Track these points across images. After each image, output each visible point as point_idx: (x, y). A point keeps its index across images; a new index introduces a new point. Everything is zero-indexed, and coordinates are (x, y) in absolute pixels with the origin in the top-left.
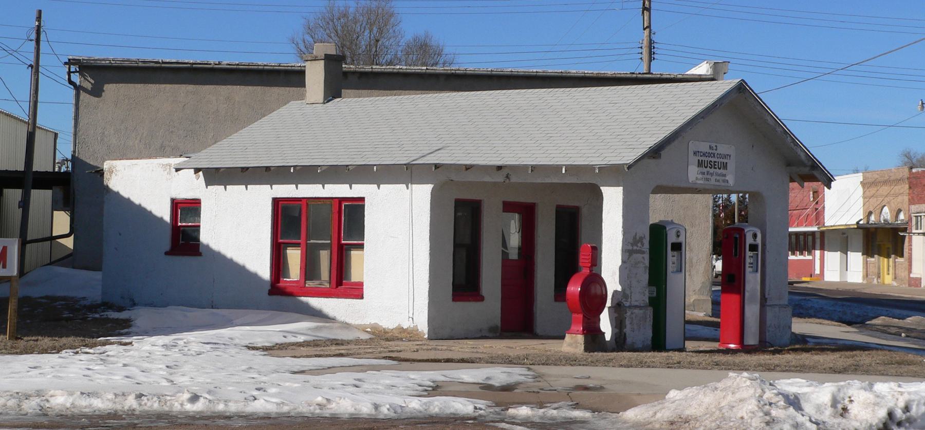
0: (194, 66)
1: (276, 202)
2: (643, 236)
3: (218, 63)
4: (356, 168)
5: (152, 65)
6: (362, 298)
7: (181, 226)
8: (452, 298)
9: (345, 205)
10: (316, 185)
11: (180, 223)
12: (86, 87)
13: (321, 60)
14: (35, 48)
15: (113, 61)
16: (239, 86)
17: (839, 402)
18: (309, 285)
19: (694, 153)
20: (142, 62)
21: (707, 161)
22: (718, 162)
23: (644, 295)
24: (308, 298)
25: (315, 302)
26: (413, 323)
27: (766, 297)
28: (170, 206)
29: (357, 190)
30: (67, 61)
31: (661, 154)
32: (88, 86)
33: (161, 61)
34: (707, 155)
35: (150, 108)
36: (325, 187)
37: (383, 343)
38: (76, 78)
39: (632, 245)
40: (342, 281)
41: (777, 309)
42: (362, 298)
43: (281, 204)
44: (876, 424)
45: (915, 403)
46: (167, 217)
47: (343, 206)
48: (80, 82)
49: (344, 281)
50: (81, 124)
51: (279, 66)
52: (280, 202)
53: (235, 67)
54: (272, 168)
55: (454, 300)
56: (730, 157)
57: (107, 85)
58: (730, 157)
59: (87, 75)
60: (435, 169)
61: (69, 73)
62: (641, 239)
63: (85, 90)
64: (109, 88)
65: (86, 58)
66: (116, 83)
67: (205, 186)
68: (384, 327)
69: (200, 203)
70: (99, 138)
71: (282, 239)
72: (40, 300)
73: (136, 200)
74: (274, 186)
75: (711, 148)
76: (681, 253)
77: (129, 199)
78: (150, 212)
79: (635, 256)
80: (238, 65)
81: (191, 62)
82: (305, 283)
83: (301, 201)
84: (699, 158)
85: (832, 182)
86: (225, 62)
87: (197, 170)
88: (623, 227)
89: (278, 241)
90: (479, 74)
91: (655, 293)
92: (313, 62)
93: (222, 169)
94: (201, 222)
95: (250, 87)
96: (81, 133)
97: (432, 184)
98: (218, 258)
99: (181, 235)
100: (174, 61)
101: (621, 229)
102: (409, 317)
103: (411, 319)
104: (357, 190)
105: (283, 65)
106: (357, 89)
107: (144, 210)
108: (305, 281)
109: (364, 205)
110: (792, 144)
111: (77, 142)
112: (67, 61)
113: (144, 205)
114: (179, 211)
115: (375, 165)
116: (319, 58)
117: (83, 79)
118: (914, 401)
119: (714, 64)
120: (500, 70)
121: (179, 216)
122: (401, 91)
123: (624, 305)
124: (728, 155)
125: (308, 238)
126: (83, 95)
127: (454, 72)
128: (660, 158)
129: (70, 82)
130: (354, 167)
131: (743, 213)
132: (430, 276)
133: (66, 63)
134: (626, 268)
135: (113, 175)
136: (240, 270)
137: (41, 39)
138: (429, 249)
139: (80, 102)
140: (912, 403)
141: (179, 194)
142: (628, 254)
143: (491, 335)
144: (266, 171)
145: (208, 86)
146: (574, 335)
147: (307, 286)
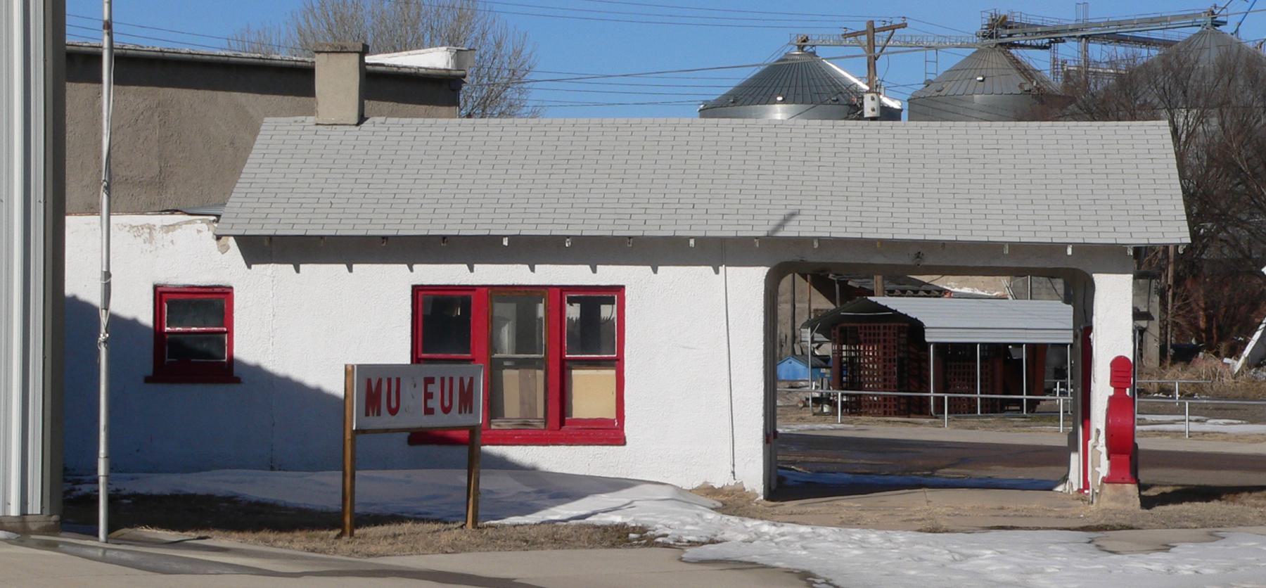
1: (417, 290)
6: (624, 443)
7: (169, 333)
9: (568, 298)
10: (515, 266)
13: (355, 52)
24: (501, 447)
26: (735, 479)
29: (607, 275)
40: (564, 418)
46: (147, 318)
47: (566, 299)
49: (567, 418)
71: (423, 353)
74: (415, 267)
82: (490, 423)
83: (475, 290)
90: (245, 62)
92: (330, 55)
97: (767, 266)
104: (607, 275)
114: (166, 306)
116: (349, 50)
119: (456, 53)
120: (172, 51)
121: (166, 315)
137: (67, 12)
146: (1120, 485)
147: (493, 427)
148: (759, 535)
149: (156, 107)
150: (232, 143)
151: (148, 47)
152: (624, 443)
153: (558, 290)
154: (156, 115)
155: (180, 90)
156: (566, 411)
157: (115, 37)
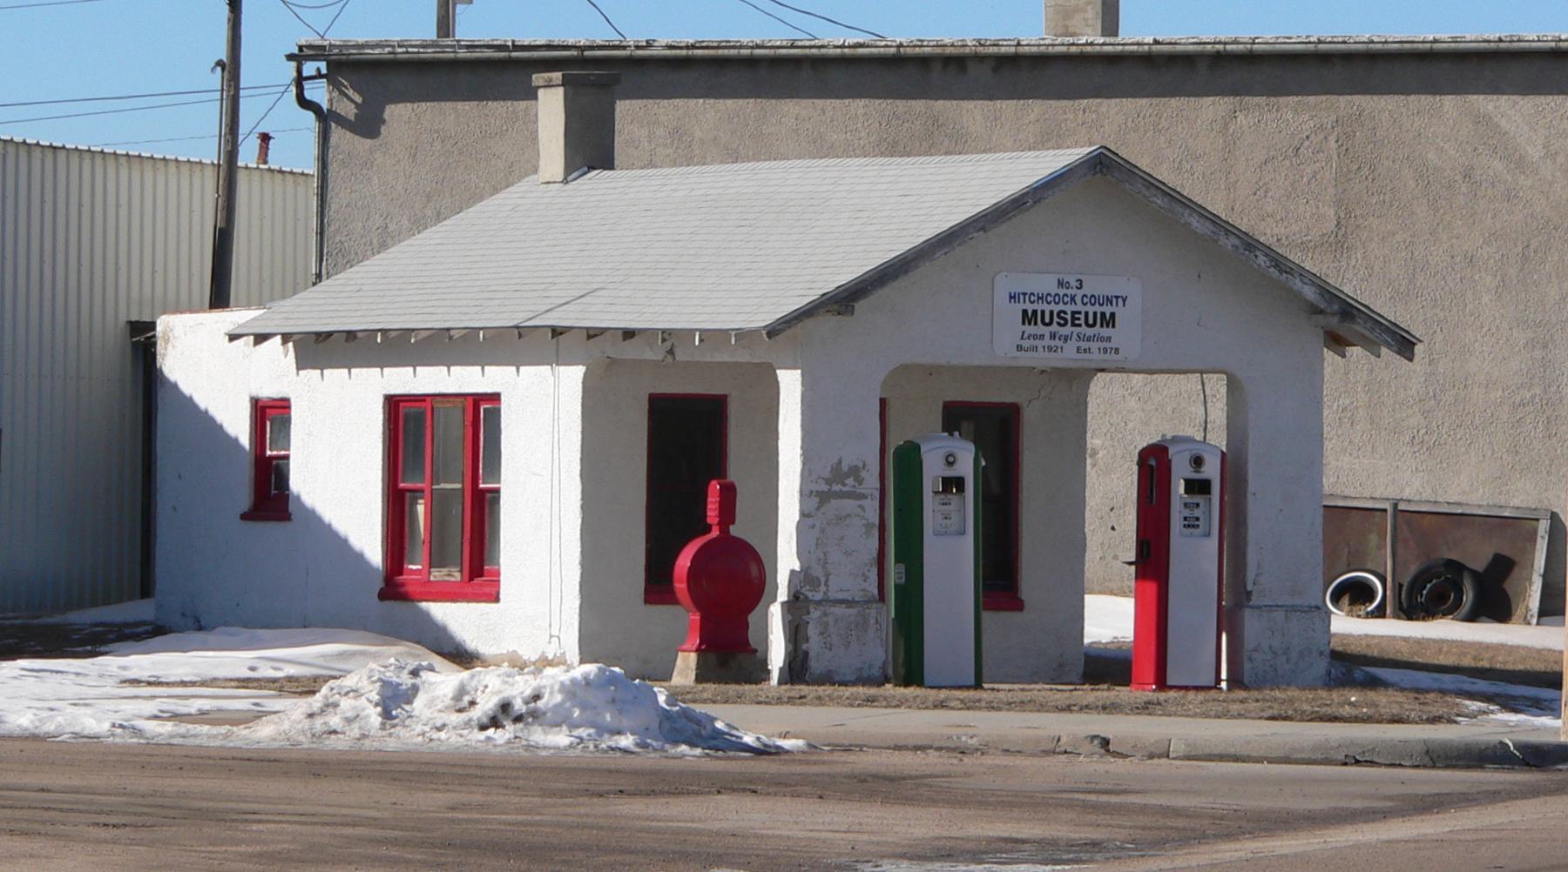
0: (587, 53)
1: (394, 405)
2: (861, 465)
3: (644, 44)
4: (300, 339)
5: (489, 54)
6: (496, 599)
8: (643, 597)
9: (485, 410)
11: (271, 450)
12: (343, 114)
14: (229, 20)
15: (400, 46)
16: (701, 101)
17: (468, 693)
18: (435, 577)
19: (1011, 297)
20: (468, 47)
21: (1095, 314)
22: (1087, 313)
23: (865, 581)
25: (440, 611)
27: (1249, 589)
28: (248, 414)
30: (296, 51)
31: (853, 306)
32: (348, 110)
33: (510, 44)
34: (1049, 299)
35: (493, 162)
36: (385, 374)
38: (318, 92)
39: (828, 481)
40: (483, 567)
41: (1279, 615)
42: (496, 599)
43: (404, 407)
44: (479, 719)
45: (548, 690)
46: (245, 440)
48: (331, 101)
49: (486, 567)
50: (332, 206)
51: (792, 47)
52: (401, 404)
53: (684, 52)
54: (360, 335)
55: (646, 601)
56: (1124, 301)
57: (393, 106)
58: (1124, 301)
59: (346, 83)
60: (553, 337)
61: (300, 80)
62: (855, 472)
63: (342, 121)
64: (396, 113)
65: (338, 43)
66: (412, 101)
67: (295, 370)
68: (525, 658)
69: (289, 407)
70: (375, 241)
73: (202, 402)
74: (522, 369)
75: (1060, 284)
76: (1210, 499)
77: (190, 399)
78: (221, 427)
79: (834, 503)
80: (693, 47)
81: (582, 44)
82: (430, 573)
83: (424, 400)
85: (1416, 347)
86: (663, 41)
87: (286, 338)
88: (802, 448)
89: (478, 485)
91: (903, 580)
93: (393, 334)
94: (292, 448)
95: (729, 102)
96: (332, 228)
98: (312, 518)
99: (273, 477)
100: (543, 43)
101: (799, 451)
102: (551, 636)
103: (555, 640)
105: (800, 44)
106: (990, 99)
107: (212, 420)
108: (430, 567)
109: (499, 411)
110: (1272, 269)
111: (325, 251)
112: (296, 51)
113: (213, 412)
114: (268, 424)
115: (481, 329)
117: (335, 94)
118: (545, 687)
122: (1099, 100)
123: (806, 597)
124: (1117, 297)
125: (434, 479)
126: (338, 134)
127: (1220, 47)
128: (853, 314)
129: (304, 103)
130: (464, 332)
132: (582, 552)
133: (290, 57)
134: (813, 527)
135: (170, 347)
136: (341, 544)
138: (579, 497)
139: (331, 150)
140: (543, 691)
141: (261, 388)
142: (817, 499)
144: (346, 341)
145: (627, 102)
148: (767, 737)
149: (1333, 128)
150: (1467, 176)
151: (1299, 37)
152: (646, 601)
153: (470, 399)
154: (1332, 139)
155: (1375, 98)
156: (486, 556)
157: (541, 84)
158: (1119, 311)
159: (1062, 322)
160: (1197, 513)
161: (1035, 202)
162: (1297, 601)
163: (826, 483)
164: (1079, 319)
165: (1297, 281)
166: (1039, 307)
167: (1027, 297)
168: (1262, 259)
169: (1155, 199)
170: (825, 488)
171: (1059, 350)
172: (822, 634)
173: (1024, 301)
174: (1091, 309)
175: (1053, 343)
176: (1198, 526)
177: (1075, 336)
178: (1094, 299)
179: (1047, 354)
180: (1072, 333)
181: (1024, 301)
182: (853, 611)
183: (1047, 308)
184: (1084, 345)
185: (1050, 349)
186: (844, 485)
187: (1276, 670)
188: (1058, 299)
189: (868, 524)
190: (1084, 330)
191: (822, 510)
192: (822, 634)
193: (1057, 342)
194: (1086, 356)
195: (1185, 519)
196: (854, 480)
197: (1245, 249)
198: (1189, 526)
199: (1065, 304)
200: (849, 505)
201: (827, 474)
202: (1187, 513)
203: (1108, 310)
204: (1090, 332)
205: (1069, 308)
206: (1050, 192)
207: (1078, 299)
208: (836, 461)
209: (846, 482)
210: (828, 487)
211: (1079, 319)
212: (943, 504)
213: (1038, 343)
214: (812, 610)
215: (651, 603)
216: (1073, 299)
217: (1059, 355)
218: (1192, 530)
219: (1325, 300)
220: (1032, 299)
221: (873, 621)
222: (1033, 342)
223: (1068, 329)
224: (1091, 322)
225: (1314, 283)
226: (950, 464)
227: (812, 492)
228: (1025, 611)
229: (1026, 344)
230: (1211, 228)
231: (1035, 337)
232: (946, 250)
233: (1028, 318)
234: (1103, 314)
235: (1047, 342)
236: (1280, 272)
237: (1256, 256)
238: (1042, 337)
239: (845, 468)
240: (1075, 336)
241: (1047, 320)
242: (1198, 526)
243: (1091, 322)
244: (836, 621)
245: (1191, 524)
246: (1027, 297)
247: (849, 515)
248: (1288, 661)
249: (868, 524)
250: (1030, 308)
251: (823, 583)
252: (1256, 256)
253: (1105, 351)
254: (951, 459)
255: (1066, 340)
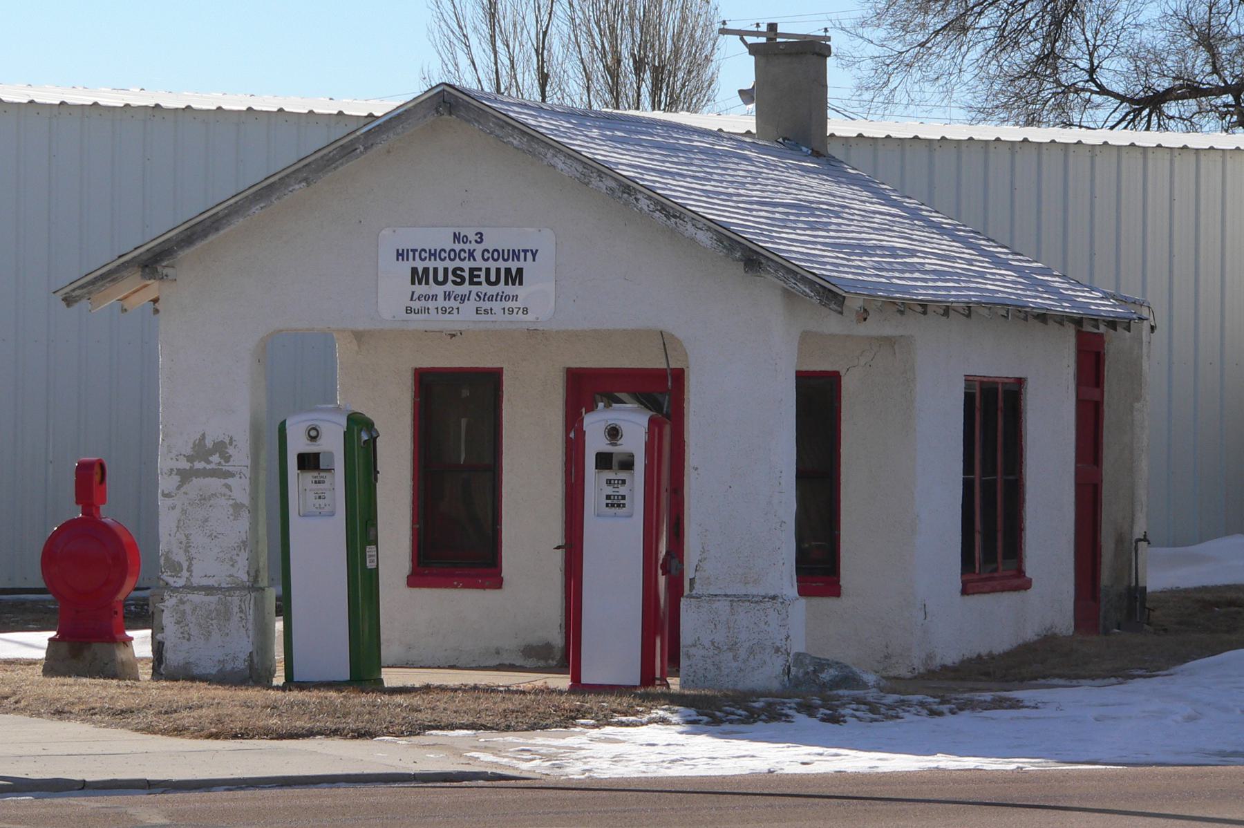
2: (227, 441)
19: (398, 254)
21: (498, 270)
22: (488, 270)
23: (233, 565)
37: (357, 701)
39: (190, 459)
41: (722, 606)
56: (534, 255)
72: (992, 266)
75: (457, 238)
84: (414, 264)
124: (525, 251)
131: (465, 393)
142: (178, 478)
143: (529, 663)
158: (527, 265)
159: (459, 280)
160: (622, 490)
161: (366, 149)
162: (752, 590)
163: (188, 461)
164: (479, 276)
165: (689, 226)
166: (431, 264)
167: (417, 254)
168: (644, 203)
169: (511, 139)
170: (187, 466)
171: (455, 311)
172: (178, 623)
173: (414, 259)
174: (492, 265)
175: (447, 304)
176: (624, 505)
177: (473, 296)
178: (497, 254)
179: (441, 316)
180: (470, 292)
181: (414, 259)
182: (213, 599)
183: (441, 266)
184: (487, 305)
185: (444, 310)
186: (209, 462)
187: (719, 668)
188: (454, 255)
189: (236, 503)
190: (485, 288)
191: (183, 490)
192: (178, 623)
193: (452, 303)
194: (489, 317)
195: (608, 497)
196: (221, 457)
197: (623, 192)
198: (613, 505)
199: (462, 260)
200: (215, 483)
201: (188, 451)
202: (609, 490)
203: (514, 265)
204: (492, 290)
205: (467, 265)
206: (384, 137)
207: (478, 255)
208: (198, 436)
209: (211, 458)
210: (190, 464)
211: (479, 276)
212: (316, 482)
213: (431, 304)
214: (166, 597)
215: (411, 587)
216: (471, 254)
217: (455, 316)
218: (613, 510)
219: (725, 247)
220: (423, 255)
221: (236, 610)
222: (423, 303)
223: (466, 288)
224: (493, 279)
225: (709, 229)
226: (313, 439)
227: (172, 470)
228: (843, 597)
229: (416, 305)
230: (580, 169)
231: (427, 298)
232: (262, 205)
233: (418, 277)
234: (508, 271)
235: (441, 302)
236: (668, 216)
237: (637, 200)
238: (435, 297)
239: (209, 443)
240: (473, 296)
241: (441, 278)
242: (624, 505)
243: (493, 279)
244: (194, 610)
245: (615, 502)
246: (417, 254)
247: (214, 495)
248: (735, 658)
249: (236, 503)
250: (420, 266)
251: (185, 567)
252: (637, 200)
253: (511, 311)
254: (313, 433)
255: (463, 300)
